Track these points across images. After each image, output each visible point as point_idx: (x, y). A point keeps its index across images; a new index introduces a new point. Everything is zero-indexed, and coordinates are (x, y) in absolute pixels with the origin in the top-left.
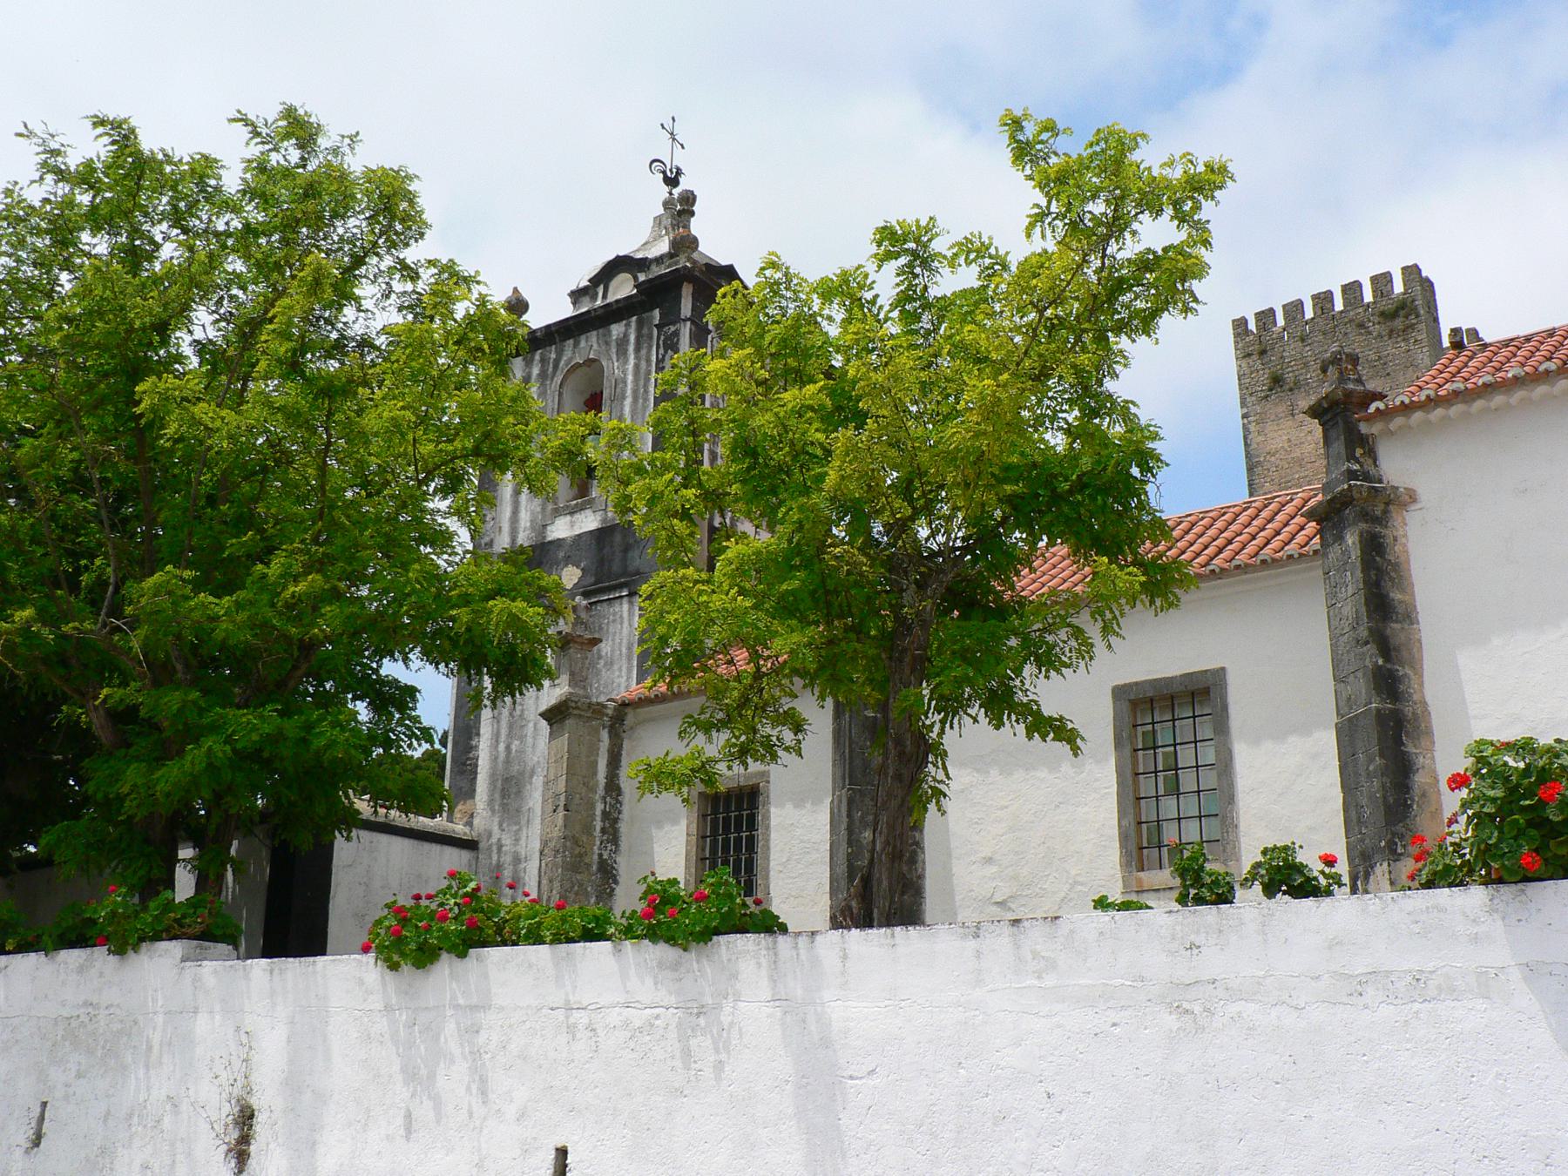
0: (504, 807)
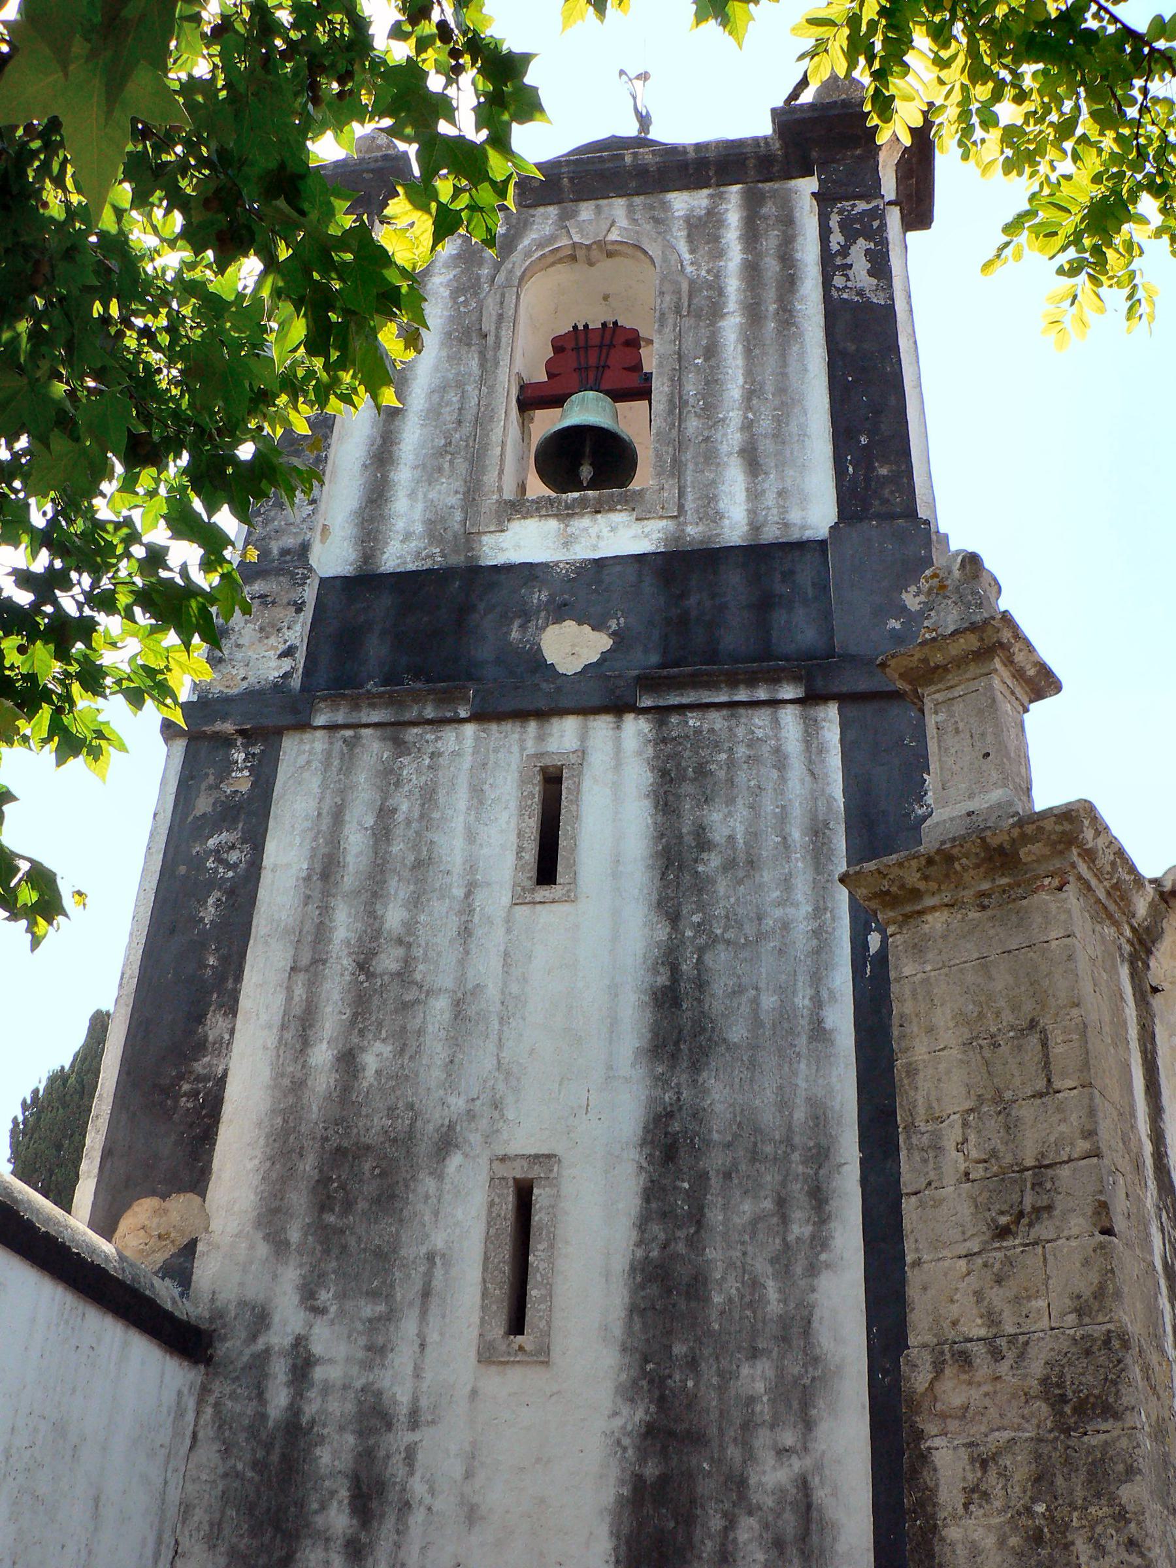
0: (327, 1239)
